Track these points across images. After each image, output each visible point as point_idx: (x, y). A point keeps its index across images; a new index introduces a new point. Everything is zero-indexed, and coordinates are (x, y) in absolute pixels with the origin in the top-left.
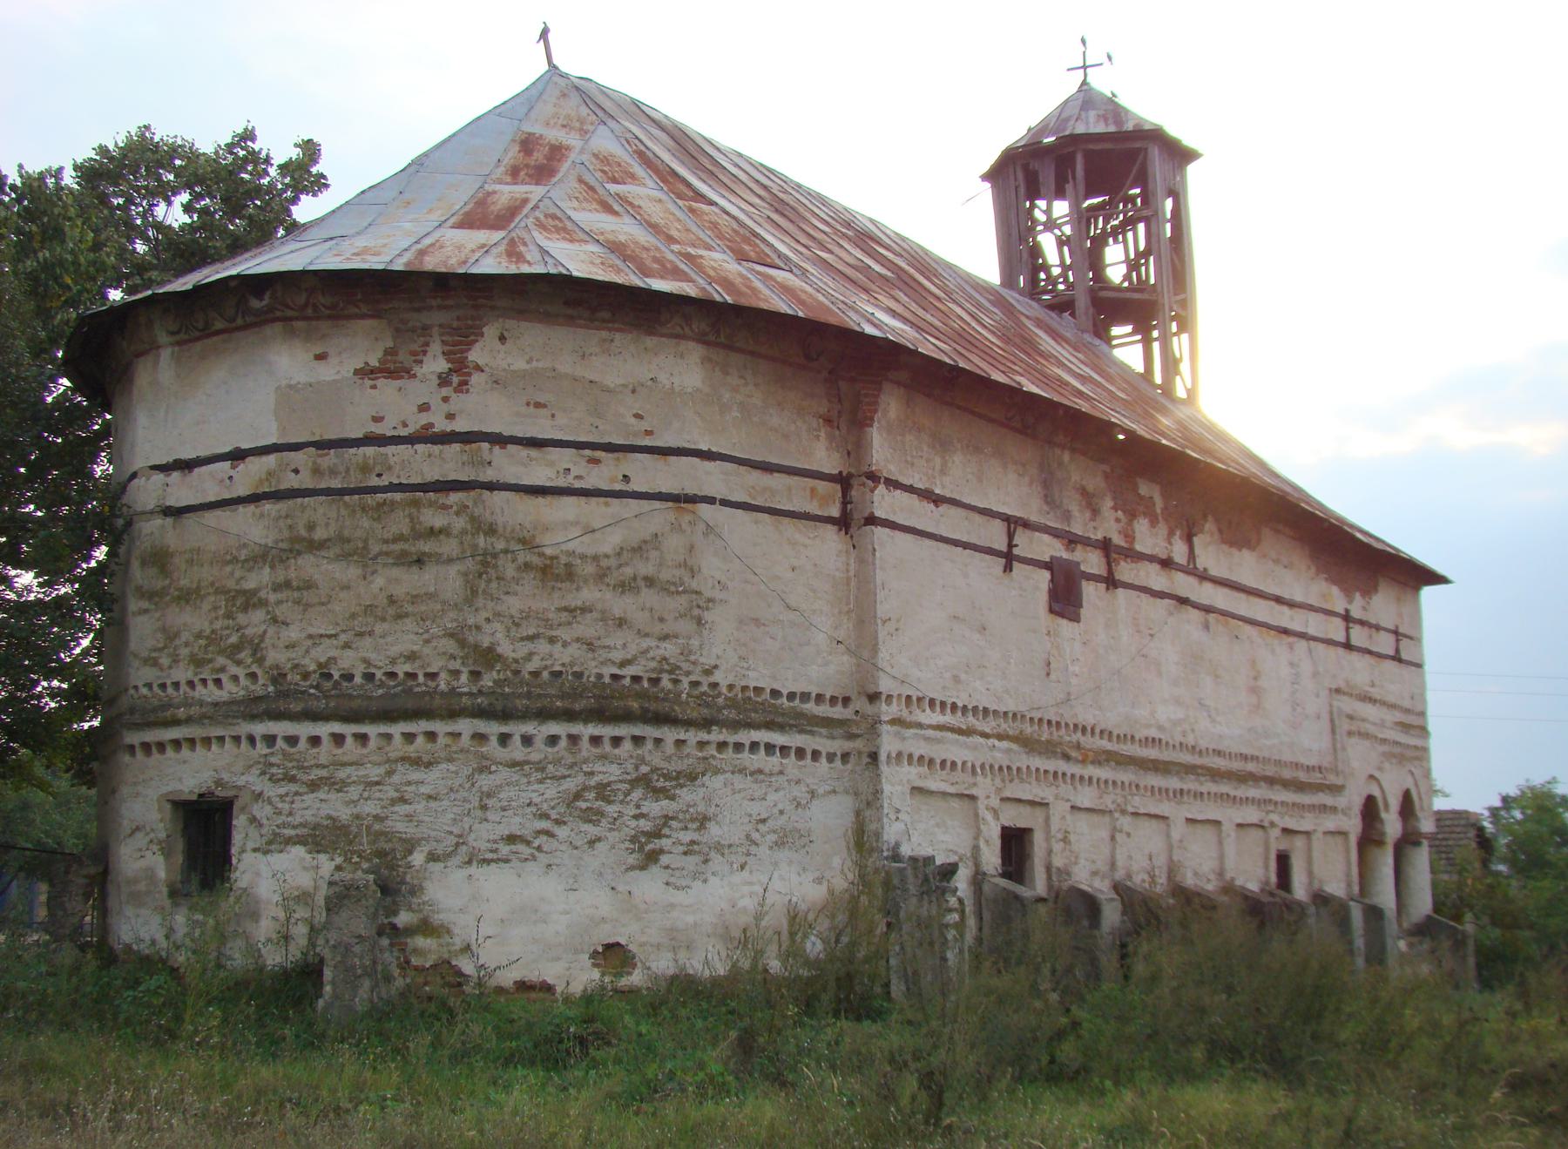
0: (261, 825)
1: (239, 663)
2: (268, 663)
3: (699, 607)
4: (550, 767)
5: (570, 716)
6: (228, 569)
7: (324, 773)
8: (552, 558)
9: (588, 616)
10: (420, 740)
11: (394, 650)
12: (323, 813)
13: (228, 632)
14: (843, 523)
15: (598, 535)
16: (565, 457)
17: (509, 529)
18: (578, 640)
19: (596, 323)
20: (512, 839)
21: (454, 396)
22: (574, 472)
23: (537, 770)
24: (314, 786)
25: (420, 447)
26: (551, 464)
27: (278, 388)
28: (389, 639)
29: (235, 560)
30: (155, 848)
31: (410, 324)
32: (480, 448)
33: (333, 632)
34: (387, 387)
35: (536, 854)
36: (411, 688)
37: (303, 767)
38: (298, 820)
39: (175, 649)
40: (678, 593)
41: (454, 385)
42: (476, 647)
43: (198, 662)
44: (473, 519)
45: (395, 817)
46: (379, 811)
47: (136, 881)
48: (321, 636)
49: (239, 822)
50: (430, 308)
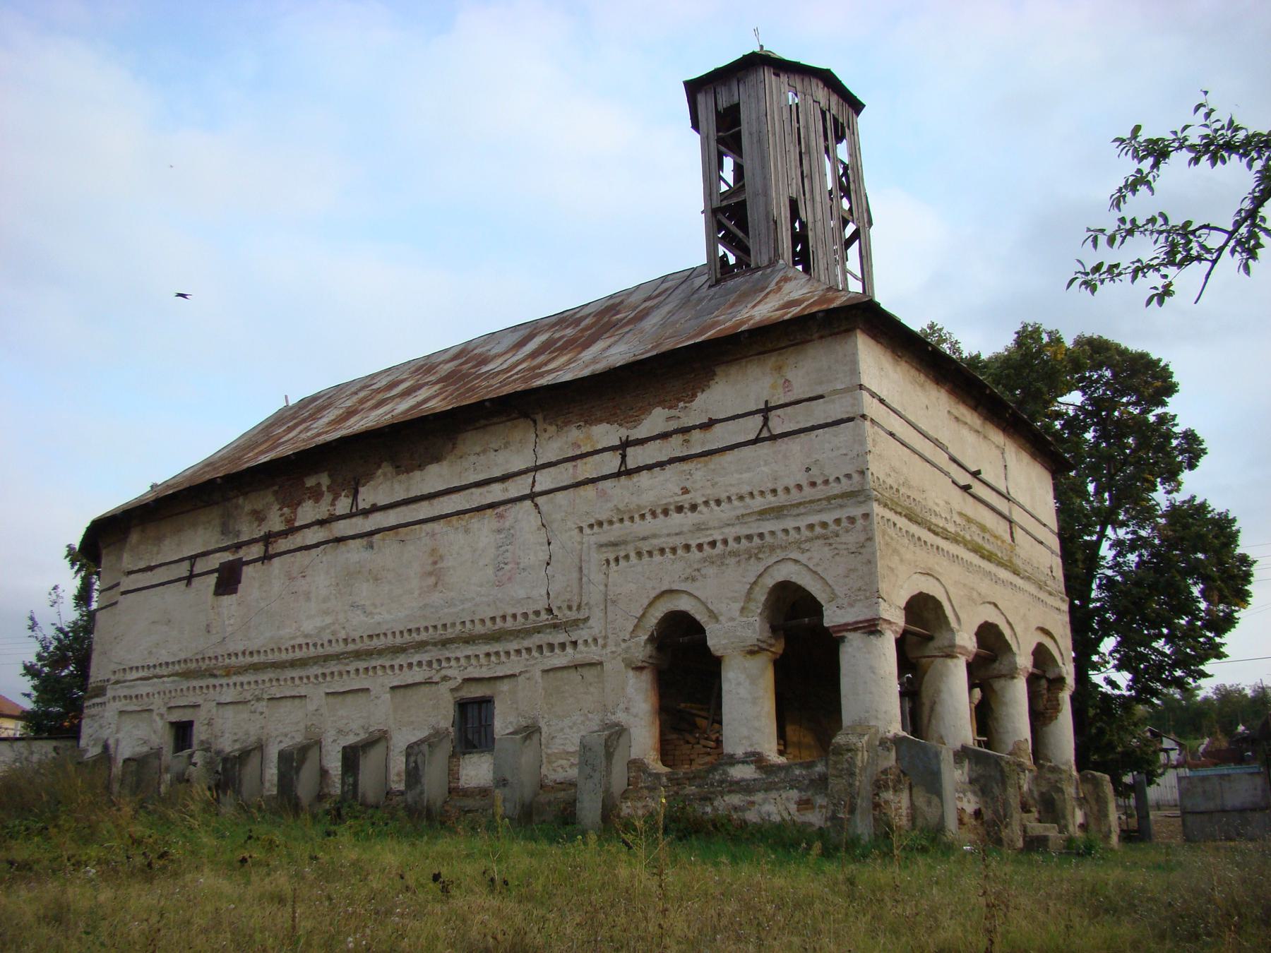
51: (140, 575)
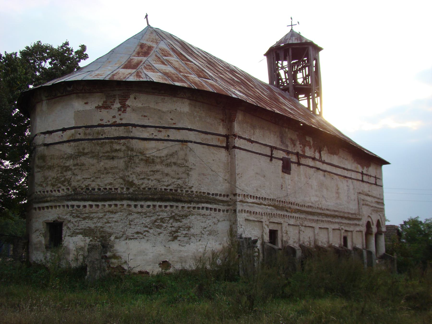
0: (70, 229)
1: (64, 186)
2: (72, 186)
3: (188, 170)
4: (148, 213)
5: (153, 200)
6: (61, 160)
7: (87, 215)
8: (148, 157)
9: (158, 173)
10: (113, 206)
11: (106, 182)
12: (87, 226)
13: (61, 177)
14: (227, 148)
15: (161, 151)
16: (152, 130)
18: (155, 179)
20: (138, 233)
23: (145, 214)
24: (84, 219)
25: (113, 128)
26: (148, 132)
27: (75, 112)
28: (105, 179)
29: (63, 158)
30: (42, 235)
32: (129, 128)
33: (89, 177)
35: (144, 237)
37: (81, 214)
38: (80, 228)
39: (47, 182)
40: (182, 167)
41: (122, 111)
42: (128, 181)
43: (53, 185)
44: (127, 147)
45: (106, 227)
46: (102, 225)
48: (86, 178)
49: (64, 228)
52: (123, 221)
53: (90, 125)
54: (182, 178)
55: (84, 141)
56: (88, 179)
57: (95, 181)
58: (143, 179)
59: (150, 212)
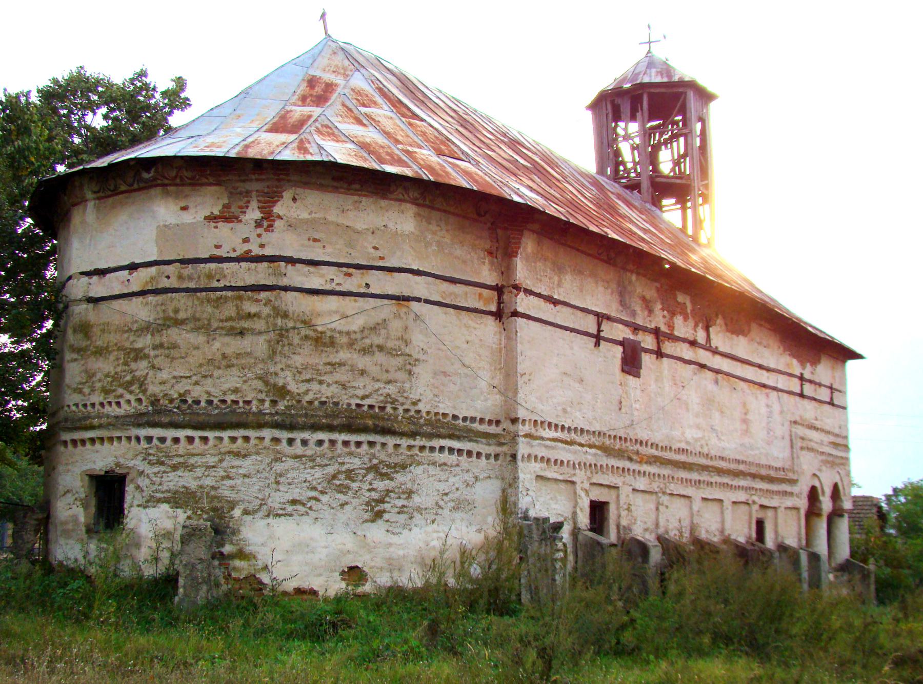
0: (143, 491)
1: (131, 392)
2: (148, 393)
3: (410, 364)
5: (330, 428)
6: (126, 335)
7: (181, 460)
8: (322, 333)
9: (343, 368)
10: (240, 441)
11: (226, 387)
12: (180, 484)
14: (498, 315)
15: (349, 319)
17: (296, 315)
18: (336, 382)
19: (351, 191)
20: (294, 502)
21: (264, 234)
22: (336, 281)
23: (310, 461)
24: (175, 468)
25: (243, 264)
26: (322, 276)
27: (158, 227)
28: (222, 380)
29: (130, 330)
30: (78, 503)
31: (239, 190)
32: (279, 266)
33: (188, 375)
34: (224, 228)
35: (309, 511)
36: (235, 410)
37: (169, 456)
38: (165, 488)
39: (93, 383)
40: (397, 355)
41: (265, 227)
42: (275, 385)
43: (106, 392)
45: (224, 487)
46: (214, 484)
47: (66, 523)
48: (181, 377)
49: (130, 488)
50: (251, 180)
51: (540, 302)
52: (262, 475)
53: (191, 257)
54: (396, 382)
55: (177, 294)
56: (184, 380)
57: (201, 383)
58: (308, 381)
59: (324, 455)
